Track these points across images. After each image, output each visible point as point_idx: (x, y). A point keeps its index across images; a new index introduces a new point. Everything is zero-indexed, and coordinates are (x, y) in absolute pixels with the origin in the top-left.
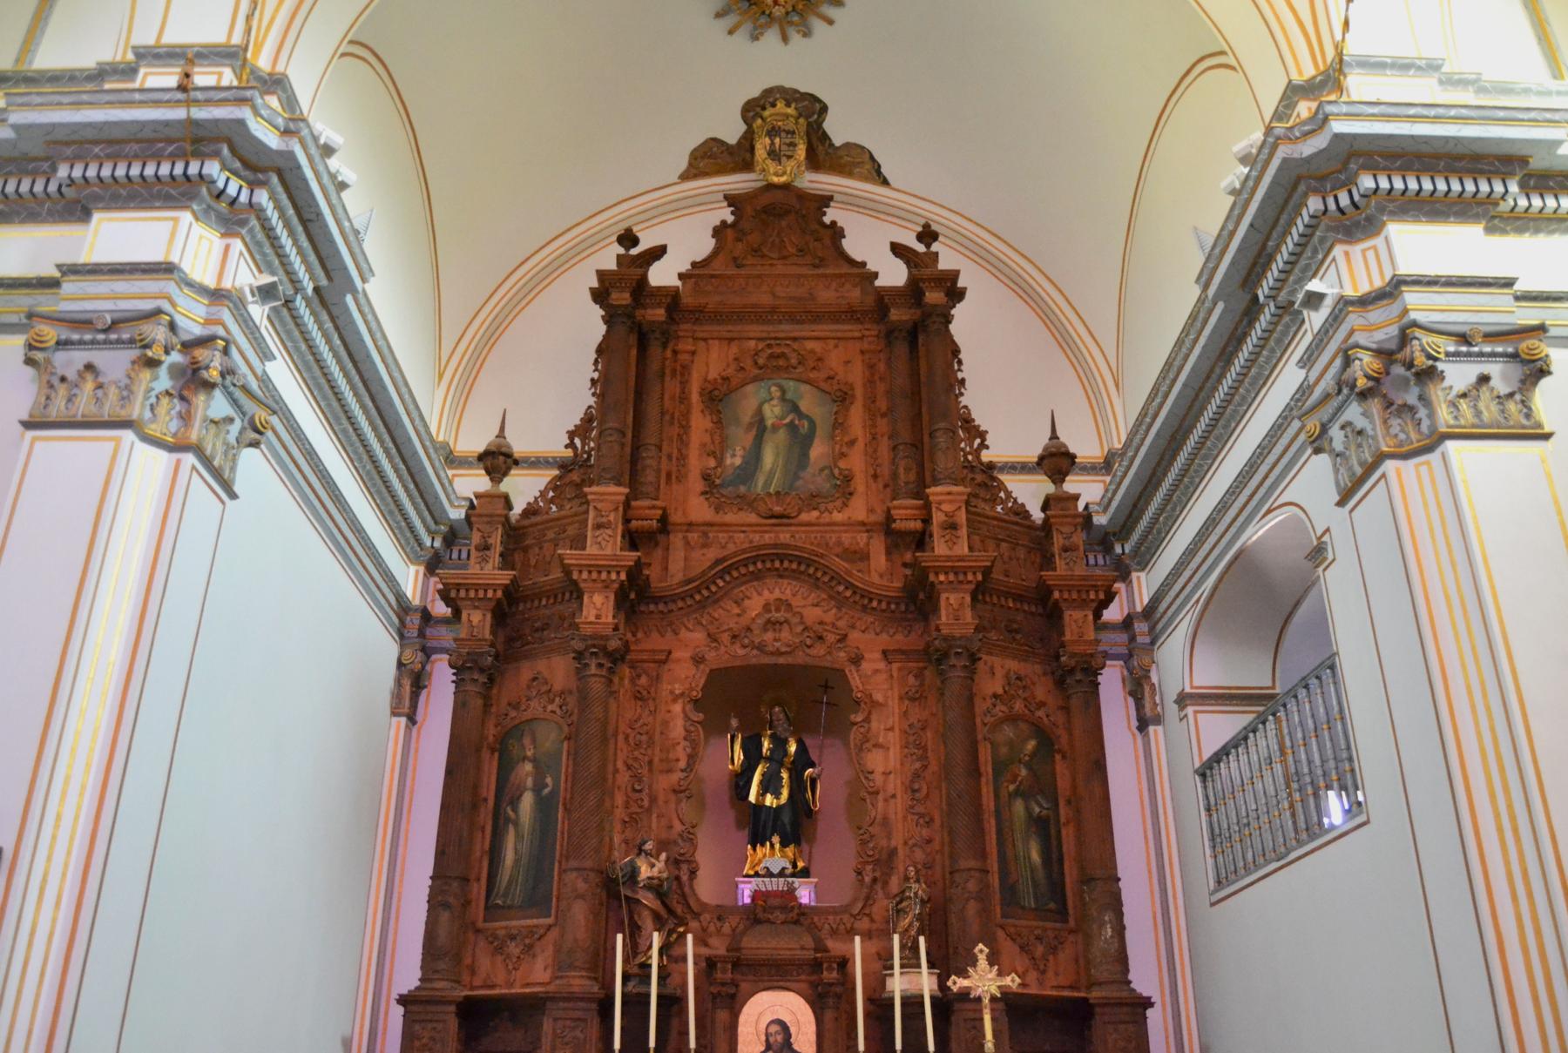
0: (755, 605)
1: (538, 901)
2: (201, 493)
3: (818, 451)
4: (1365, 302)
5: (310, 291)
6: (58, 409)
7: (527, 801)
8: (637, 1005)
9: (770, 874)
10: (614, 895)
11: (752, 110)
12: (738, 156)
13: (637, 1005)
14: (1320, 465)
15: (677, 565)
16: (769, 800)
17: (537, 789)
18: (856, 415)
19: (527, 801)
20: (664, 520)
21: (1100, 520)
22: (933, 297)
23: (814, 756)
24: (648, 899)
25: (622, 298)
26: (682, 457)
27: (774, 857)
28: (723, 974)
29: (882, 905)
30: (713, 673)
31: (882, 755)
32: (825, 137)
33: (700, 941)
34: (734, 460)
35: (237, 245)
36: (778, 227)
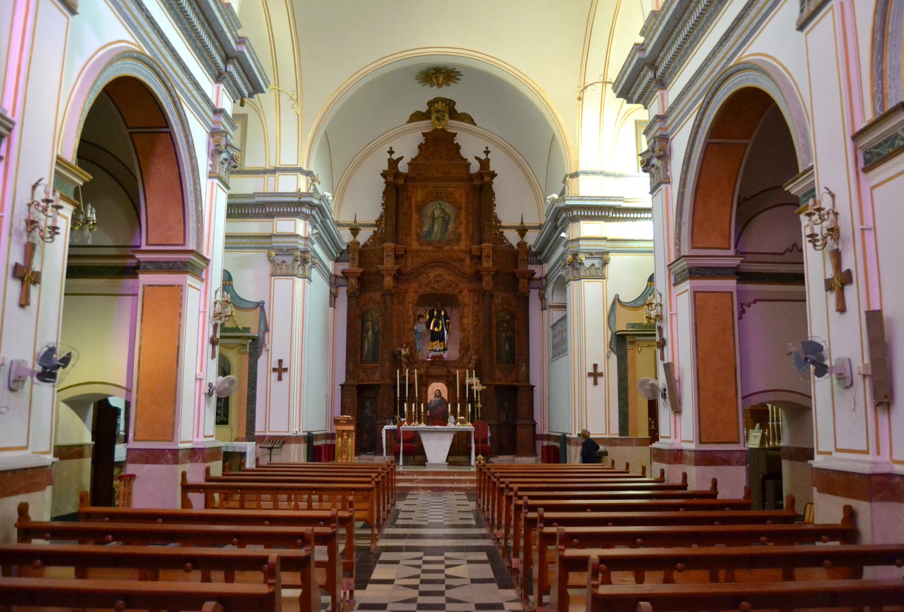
0: (432, 275)
1: (375, 359)
4: (572, 241)
6: (278, 271)
7: (370, 332)
8: (403, 386)
11: (431, 104)
12: (425, 116)
13: (403, 386)
15: (410, 264)
16: (436, 329)
17: (373, 330)
18: (463, 213)
19: (370, 332)
20: (406, 251)
21: (533, 250)
22: (487, 179)
23: (449, 315)
24: (404, 359)
25: (391, 179)
26: (410, 228)
28: (424, 379)
29: (466, 360)
30: (420, 296)
34: (426, 229)
35: (222, 86)
36: (439, 146)
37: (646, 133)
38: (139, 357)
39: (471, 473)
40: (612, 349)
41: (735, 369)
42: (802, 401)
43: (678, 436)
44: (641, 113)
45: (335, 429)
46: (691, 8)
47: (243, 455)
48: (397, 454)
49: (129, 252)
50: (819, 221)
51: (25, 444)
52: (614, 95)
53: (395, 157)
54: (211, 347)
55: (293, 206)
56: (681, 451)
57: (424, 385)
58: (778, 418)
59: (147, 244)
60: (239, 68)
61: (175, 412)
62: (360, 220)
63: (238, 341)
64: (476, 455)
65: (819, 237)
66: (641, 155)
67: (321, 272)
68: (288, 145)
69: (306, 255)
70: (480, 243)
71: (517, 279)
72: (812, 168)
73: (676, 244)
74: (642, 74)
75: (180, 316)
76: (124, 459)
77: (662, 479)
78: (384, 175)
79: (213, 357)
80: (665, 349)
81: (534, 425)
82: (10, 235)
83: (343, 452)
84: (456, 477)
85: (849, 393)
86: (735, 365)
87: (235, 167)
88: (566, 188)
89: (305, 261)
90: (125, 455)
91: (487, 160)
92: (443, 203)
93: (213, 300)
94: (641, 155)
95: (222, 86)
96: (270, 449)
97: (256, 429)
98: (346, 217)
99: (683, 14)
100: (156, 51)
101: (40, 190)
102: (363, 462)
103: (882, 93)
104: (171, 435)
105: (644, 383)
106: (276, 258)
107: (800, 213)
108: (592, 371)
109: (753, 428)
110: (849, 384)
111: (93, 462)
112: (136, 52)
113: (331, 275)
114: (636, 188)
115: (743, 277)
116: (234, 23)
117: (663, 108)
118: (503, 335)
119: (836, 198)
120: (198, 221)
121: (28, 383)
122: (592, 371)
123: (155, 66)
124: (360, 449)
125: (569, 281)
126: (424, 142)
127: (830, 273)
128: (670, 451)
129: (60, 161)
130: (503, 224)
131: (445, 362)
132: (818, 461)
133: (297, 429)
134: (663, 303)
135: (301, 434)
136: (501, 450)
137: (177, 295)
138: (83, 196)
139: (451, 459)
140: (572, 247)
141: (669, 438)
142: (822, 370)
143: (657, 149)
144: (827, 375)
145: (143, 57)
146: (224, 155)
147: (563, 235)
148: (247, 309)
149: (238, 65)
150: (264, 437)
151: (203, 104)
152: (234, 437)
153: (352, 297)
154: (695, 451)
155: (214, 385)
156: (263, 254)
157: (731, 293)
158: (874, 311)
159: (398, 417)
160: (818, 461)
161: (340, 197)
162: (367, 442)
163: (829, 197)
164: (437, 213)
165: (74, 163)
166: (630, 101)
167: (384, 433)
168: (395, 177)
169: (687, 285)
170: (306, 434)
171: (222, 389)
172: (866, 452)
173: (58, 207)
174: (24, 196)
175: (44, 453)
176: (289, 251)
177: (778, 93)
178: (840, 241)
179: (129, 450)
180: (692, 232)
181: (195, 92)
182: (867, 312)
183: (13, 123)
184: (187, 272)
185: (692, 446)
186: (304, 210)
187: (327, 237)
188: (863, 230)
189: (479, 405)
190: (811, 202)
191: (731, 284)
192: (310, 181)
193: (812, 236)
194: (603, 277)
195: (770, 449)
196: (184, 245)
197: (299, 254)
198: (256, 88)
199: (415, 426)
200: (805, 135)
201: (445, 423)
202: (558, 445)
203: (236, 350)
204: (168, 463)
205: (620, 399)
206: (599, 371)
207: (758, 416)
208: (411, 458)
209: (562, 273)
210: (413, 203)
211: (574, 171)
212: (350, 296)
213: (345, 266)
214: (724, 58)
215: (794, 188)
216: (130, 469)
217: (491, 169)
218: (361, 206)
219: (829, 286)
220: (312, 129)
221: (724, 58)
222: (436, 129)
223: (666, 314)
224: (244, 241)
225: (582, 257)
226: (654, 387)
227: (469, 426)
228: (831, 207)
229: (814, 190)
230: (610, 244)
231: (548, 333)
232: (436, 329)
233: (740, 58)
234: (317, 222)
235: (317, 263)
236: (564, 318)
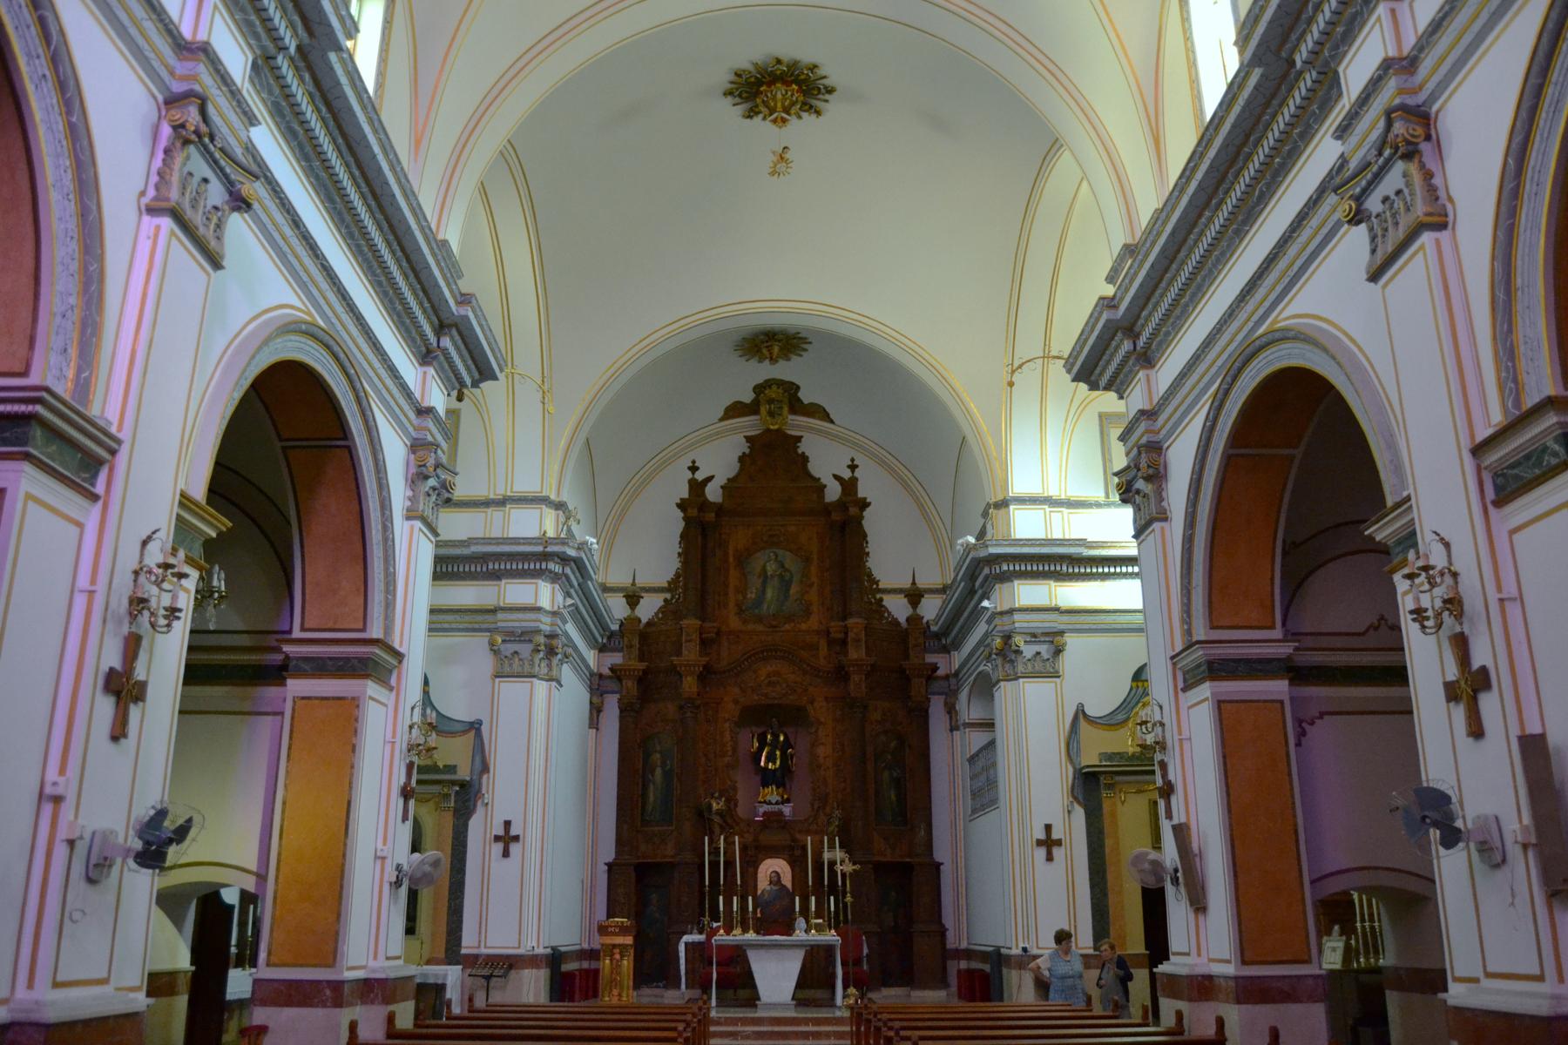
2: (183, 256)
3: (793, 590)
4: (1001, 613)
5: (292, 50)
6: (507, 669)
7: (658, 771)
8: (714, 865)
9: (770, 803)
10: (702, 817)
11: (759, 389)
13: (714, 865)
14: (1356, 239)
16: (770, 766)
17: (663, 764)
18: (813, 569)
19: (658, 771)
20: (718, 633)
21: (934, 628)
22: (853, 511)
24: (717, 819)
25: (693, 512)
26: (726, 594)
27: (771, 793)
31: (821, 745)
32: (799, 400)
33: (741, 836)
34: (751, 595)
36: (773, 456)
37: (1123, 438)
38: (283, 820)
39: (838, 1021)
40: (1075, 798)
41: (1296, 832)
42: (1412, 885)
43: (1204, 952)
44: (1108, 401)
45: (597, 942)
46: (1190, 242)
47: (440, 988)
48: (706, 988)
49: (271, 641)
50: (1427, 587)
51: (105, 975)
52: (1068, 377)
53: (700, 476)
54: (401, 801)
55: (532, 561)
56: (1210, 978)
57: (751, 864)
58: (1371, 915)
59: (303, 629)
60: (460, 342)
61: (339, 915)
62: (640, 582)
63: (435, 789)
64: (845, 987)
65: (1430, 613)
66: (1116, 474)
67: (576, 669)
68: (527, 460)
69: (554, 642)
70: (844, 618)
71: (908, 679)
72: (1408, 498)
73: (1183, 621)
74: (1114, 343)
75: (354, 751)
76: (248, 995)
77: (1179, 1029)
78: (682, 505)
79: (405, 818)
80: (1173, 799)
81: (943, 932)
82: (104, 621)
83: (613, 983)
84: (811, 1028)
85: (1499, 875)
86: (1296, 825)
87: (446, 499)
88: (989, 526)
89: (551, 652)
90: (249, 989)
91: (854, 481)
92: (780, 552)
93: (408, 722)
94: (1116, 474)
95: (431, 371)
96: (488, 978)
97: (464, 943)
98: (618, 575)
99: (1178, 251)
100: (334, 320)
101: (153, 547)
102: (645, 1000)
103: (1515, 381)
104: (331, 957)
105: (1139, 858)
106: (502, 647)
107: (1393, 571)
108: (1042, 836)
109: (1329, 933)
110: (1499, 859)
111: (190, 1002)
112: (306, 323)
113: (592, 674)
114: (1113, 527)
115: (1298, 674)
116: (453, 269)
117: (1151, 399)
118: (886, 774)
119: (1454, 548)
120: (387, 591)
121: (115, 870)
122: (1042, 836)
123: (332, 343)
124: (642, 978)
125: (998, 681)
126: (747, 451)
127: (1452, 673)
128: (1191, 978)
129: (185, 501)
130: (881, 586)
131: (786, 822)
132: (1457, 994)
133: (534, 944)
134: (1165, 721)
135: (540, 951)
136: (887, 979)
137: (348, 715)
138: (213, 551)
139: (800, 995)
140: (1002, 624)
141: (1188, 954)
142: (1452, 838)
143: (1143, 464)
144: (1461, 845)
145: (316, 330)
146: (432, 482)
147: (986, 603)
148: (452, 734)
149: (457, 337)
150: (476, 957)
151: (402, 401)
152: (426, 957)
153: (627, 711)
154: (1236, 978)
155: (405, 867)
156: (481, 641)
157: (1282, 702)
158: (1533, 736)
159: (706, 920)
160: (1457, 994)
161: (609, 546)
162: (654, 967)
163: (1441, 547)
164: (771, 568)
165: (204, 502)
166: (1094, 386)
167: (682, 948)
168: (717, 515)
169: (1205, 690)
170: (549, 951)
171: (418, 875)
172: (1540, 978)
173: (182, 576)
174: (128, 560)
175: (132, 989)
176: (525, 636)
177: (1343, 378)
178: (1465, 620)
179: (256, 982)
180: (1210, 602)
181: (389, 382)
182: (1521, 738)
183: (119, 442)
184: (366, 676)
185: (1230, 970)
186: (551, 566)
187: (588, 611)
188: (1501, 600)
189: (849, 899)
190: (1411, 555)
191: (1278, 688)
192: (562, 519)
193: (1419, 614)
194: (1056, 675)
195: (1359, 971)
196: (363, 630)
197: (541, 639)
198: (484, 373)
199: (737, 936)
200: (1392, 445)
201: (789, 930)
202: (987, 968)
203: (431, 804)
204: (325, 1006)
205: (1092, 887)
206: (1055, 836)
207: (1336, 912)
208: (730, 993)
209: (988, 668)
210: (731, 552)
211: (1000, 497)
212: (624, 710)
213: (616, 659)
214: (1248, 320)
215: (1381, 532)
216: (260, 1015)
217: (860, 495)
218: (642, 558)
219: (1452, 693)
220: (567, 433)
221: (1248, 320)
222: (768, 430)
223: (1171, 738)
224: (450, 617)
225: (1018, 640)
226: (1157, 866)
227: (831, 937)
228: (1446, 564)
229: (1414, 533)
230: (1065, 618)
231: (963, 771)
232: (770, 766)
233: (1275, 321)
234: (572, 586)
235: (571, 655)
236: (992, 744)
